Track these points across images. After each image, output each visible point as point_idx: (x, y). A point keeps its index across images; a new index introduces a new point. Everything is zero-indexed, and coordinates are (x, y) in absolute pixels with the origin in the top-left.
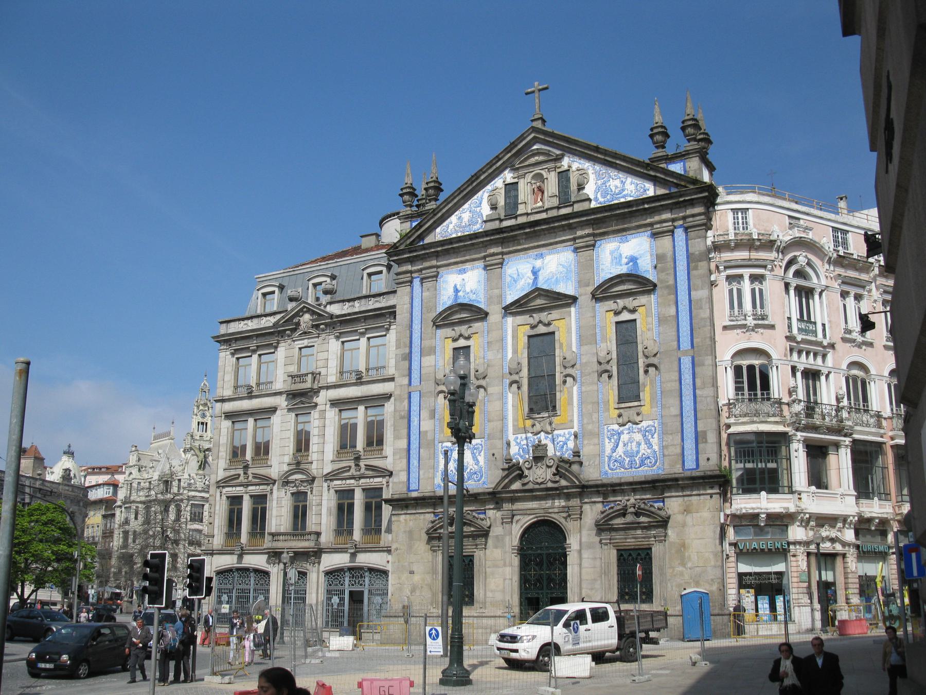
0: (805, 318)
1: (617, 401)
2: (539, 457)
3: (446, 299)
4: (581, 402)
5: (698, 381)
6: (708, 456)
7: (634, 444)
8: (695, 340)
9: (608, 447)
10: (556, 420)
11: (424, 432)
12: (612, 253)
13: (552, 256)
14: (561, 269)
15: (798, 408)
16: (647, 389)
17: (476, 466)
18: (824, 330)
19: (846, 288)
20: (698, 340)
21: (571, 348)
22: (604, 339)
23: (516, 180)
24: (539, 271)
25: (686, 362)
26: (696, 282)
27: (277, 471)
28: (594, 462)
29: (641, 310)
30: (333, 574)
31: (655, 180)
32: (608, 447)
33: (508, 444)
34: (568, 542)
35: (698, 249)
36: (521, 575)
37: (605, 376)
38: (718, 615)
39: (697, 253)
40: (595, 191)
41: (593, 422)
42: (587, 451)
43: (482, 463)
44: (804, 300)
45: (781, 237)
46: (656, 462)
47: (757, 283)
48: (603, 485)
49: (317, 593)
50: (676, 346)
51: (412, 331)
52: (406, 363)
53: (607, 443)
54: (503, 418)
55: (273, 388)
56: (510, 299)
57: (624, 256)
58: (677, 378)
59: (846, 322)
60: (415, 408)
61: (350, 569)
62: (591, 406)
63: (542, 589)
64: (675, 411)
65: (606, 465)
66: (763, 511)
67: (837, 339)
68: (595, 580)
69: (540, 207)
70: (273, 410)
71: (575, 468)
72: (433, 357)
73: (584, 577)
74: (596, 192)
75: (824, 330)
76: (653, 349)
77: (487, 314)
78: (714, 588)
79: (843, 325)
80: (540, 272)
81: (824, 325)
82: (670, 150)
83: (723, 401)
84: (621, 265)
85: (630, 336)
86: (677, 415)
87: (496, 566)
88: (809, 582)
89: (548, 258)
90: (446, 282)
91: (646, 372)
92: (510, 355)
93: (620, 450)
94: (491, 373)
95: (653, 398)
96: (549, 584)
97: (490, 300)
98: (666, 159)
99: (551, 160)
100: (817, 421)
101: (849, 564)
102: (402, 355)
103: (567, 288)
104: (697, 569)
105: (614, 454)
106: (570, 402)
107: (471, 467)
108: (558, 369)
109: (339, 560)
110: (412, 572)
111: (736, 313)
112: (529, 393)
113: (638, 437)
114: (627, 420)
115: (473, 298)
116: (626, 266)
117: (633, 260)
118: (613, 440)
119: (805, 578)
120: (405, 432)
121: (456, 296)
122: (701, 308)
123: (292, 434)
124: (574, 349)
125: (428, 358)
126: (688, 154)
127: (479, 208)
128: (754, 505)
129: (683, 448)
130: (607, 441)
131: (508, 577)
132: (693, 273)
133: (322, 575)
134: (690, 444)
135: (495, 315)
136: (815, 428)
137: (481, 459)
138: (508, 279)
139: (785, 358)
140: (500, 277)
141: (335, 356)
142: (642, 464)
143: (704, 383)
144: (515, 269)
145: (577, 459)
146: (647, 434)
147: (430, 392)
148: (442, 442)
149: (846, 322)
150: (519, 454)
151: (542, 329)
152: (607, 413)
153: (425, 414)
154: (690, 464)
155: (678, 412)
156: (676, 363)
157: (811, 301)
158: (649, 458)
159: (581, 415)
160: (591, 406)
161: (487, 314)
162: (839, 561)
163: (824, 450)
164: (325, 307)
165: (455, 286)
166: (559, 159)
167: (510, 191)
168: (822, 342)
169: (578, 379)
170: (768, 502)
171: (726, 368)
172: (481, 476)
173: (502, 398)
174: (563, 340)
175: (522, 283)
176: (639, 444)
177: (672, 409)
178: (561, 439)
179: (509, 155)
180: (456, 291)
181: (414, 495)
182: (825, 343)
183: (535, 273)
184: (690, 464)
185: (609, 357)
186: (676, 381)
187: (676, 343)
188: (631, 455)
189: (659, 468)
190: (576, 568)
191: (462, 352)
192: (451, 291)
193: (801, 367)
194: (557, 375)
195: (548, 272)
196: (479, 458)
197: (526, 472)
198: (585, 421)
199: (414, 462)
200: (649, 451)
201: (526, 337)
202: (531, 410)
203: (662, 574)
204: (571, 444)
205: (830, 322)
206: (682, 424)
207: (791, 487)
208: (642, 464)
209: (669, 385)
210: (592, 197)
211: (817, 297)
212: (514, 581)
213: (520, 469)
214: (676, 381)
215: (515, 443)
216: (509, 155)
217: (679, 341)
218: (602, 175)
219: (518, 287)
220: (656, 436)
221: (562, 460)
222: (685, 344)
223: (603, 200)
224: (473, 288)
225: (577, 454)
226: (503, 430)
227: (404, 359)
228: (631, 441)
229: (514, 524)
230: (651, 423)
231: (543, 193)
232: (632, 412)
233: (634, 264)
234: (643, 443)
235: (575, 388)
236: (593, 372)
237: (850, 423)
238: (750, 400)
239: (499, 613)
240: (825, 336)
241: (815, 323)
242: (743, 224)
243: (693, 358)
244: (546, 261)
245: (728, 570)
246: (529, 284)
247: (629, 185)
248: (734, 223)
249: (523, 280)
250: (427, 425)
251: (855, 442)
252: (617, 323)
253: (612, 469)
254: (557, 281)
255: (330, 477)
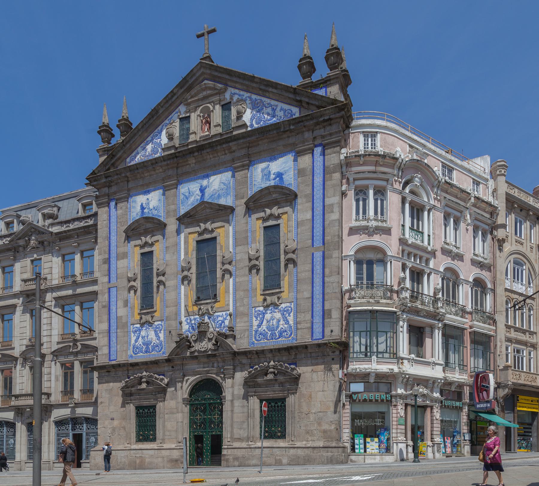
0: (415, 228)
1: (263, 288)
2: (202, 335)
3: (135, 213)
4: (235, 290)
5: (327, 271)
6: (332, 328)
7: (275, 321)
8: (325, 238)
9: (255, 323)
10: (217, 305)
11: (120, 317)
12: (263, 170)
13: (215, 176)
14: (222, 186)
15: (406, 294)
16: (286, 278)
17: (158, 341)
18: (429, 240)
19: (449, 210)
20: (328, 238)
21: (229, 249)
22: (254, 240)
23: (188, 115)
24: (205, 189)
25: (318, 255)
26: (329, 192)
27: (18, 351)
28: (244, 335)
29: (284, 217)
30: (59, 423)
31: (299, 104)
32: (255, 323)
33: (181, 323)
34: (223, 394)
35: (333, 162)
36: (190, 419)
37: (254, 271)
38: (335, 447)
39: (332, 166)
40: (251, 119)
41: (244, 305)
42: (240, 326)
43: (162, 338)
44: (415, 221)
45: (402, 157)
46: (291, 334)
47: (379, 195)
48: (250, 352)
49: (49, 436)
50: (310, 244)
51: (110, 242)
52: (106, 266)
53: (254, 321)
54: (177, 304)
55: (14, 290)
56: (182, 212)
57: (272, 172)
58: (310, 269)
59: (445, 238)
60: (113, 299)
61: (72, 419)
62: (243, 292)
63: (205, 429)
64: (307, 294)
65: (253, 337)
66: (373, 371)
67: (438, 247)
68: (244, 422)
69: (207, 135)
70: (14, 306)
71: (229, 341)
72: (125, 260)
73: (235, 420)
74: (252, 120)
75: (429, 240)
76: (292, 245)
77: (165, 225)
78: (333, 427)
79: (443, 239)
80: (206, 190)
81: (429, 236)
82: (315, 77)
83: (346, 287)
84: (270, 180)
85: (274, 237)
86: (309, 298)
87: (172, 413)
88: (406, 425)
89: (212, 178)
90: (135, 202)
91: (286, 266)
92: (182, 257)
93: (264, 327)
94: (168, 271)
95: (290, 285)
96: (205, 408)
97: (168, 213)
98: (311, 87)
99: (216, 94)
100: (418, 305)
101: (435, 414)
102: (103, 259)
103: (227, 201)
104: (320, 413)
105: (260, 329)
106: (227, 291)
107: (154, 342)
108: (219, 265)
109: (64, 413)
110: (112, 419)
111: (361, 218)
112: (197, 285)
113: (278, 315)
114: (270, 302)
115: (155, 214)
116: (274, 181)
117: (280, 175)
118: (259, 319)
119: (403, 422)
120: (106, 317)
121: (143, 212)
122: (332, 212)
123: (28, 324)
124: (231, 250)
125: (122, 261)
126: (330, 80)
127: (159, 140)
128: (366, 366)
129: (312, 323)
130: (254, 319)
131: (180, 420)
132: (328, 183)
133: (53, 426)
134: (318, 319)
135: (172, 226)
136: (417, 312)
137: (161, 335)
138: (182, 197)
139: (398, 256)
140: (175, 195)
141: (57, 265)
142: (281, 336)
143: (331, 272)
144: (187, 188)
145: (231, 333)
146: (285, 313)
147: (124, 287)
148: (134, 324)
149: (445, 238)
150: (189, 331)
151: (207, 236)
152: (255, 298)
153: (120, 303)
154: (318, 335)
155: (309, 295)
156: (311, 257)
157: (420, 222)
158: (286, 331)
159: (235, 301)
160: (243, 292)
161: (165, 225)
162: (429, 410)
163: (422, 329)
164: (48, 228)
165: (142, 205)
166: (221, 92)
167: (183, 124)
168: (427, 248)
169: (233, 273)
170: (377, 364)
171: (350, 262)
172: (162, 348)
173: (178, 289)
174: (223, 243)
175: (192, 199)
176: (279, 321)
177: (305, 293)
178: (220, 318)
179: (183, 90)
180: (143, 208)
181: (113, 363)
182: (429, 249)
183: (202, 190)
184: (318, 335)
185: (258, 255)
186: (309, 271)
187: (311, 241)
188: (272, 329)
189: (293, 339)
190: (229, 413)
191: (147, 257)
192: (139, 208)
193: (409, 264)
194: (218, 270)
195: (212, 189)
196: (160, 335)
197: (193, 344)
198: (238, 304)
199: (113, 339)
200: (286, 326)
201: (195, 242)
202: (198, 299)
203: (293, 417)
204: (227, 323)
205: (434, 233)
206: (312, 305)
207: (396, 354)
208: (281, 336)
209: (303, 275)
210: (248, 124)
211: (426, 213)
212: (184, 423)
213: (189, 341)
214: (309, 271)
215: (186, 323)
216: (183, 90)
217: (313, 240)
218: (258, 104)
219: (189, 203)
220: (292, 314)
221: (220, 334)
222: (318, 242)
223: (257, 126)
224: (155, 206)
225: (231, 329)
226: (177, 314)
227: (104, 263)
228: (272, 318)
229: (184, 382)
230: (288, 304)
231: (210, 124)
232: (275, 299)
233: (280, 179)
234: (282, 320)
235: (231, 280)
236: (245, 266)
237: (444, 311)
238: (367, 287)
239: (173, 446)
240: (429, 244)
241: (422, 233)
242: (372, 145)
243: (324, 252)
244: (211, 181)
245: (344, 419)
246: (197, 200)
247: (279, 111)
248: (365, 144)
249: (193, 197)
250: (122, 312)
251: (445, 325)
252: (265, 228)
253: (258, 341)
254: (219, 197)
255: (56, 354)
